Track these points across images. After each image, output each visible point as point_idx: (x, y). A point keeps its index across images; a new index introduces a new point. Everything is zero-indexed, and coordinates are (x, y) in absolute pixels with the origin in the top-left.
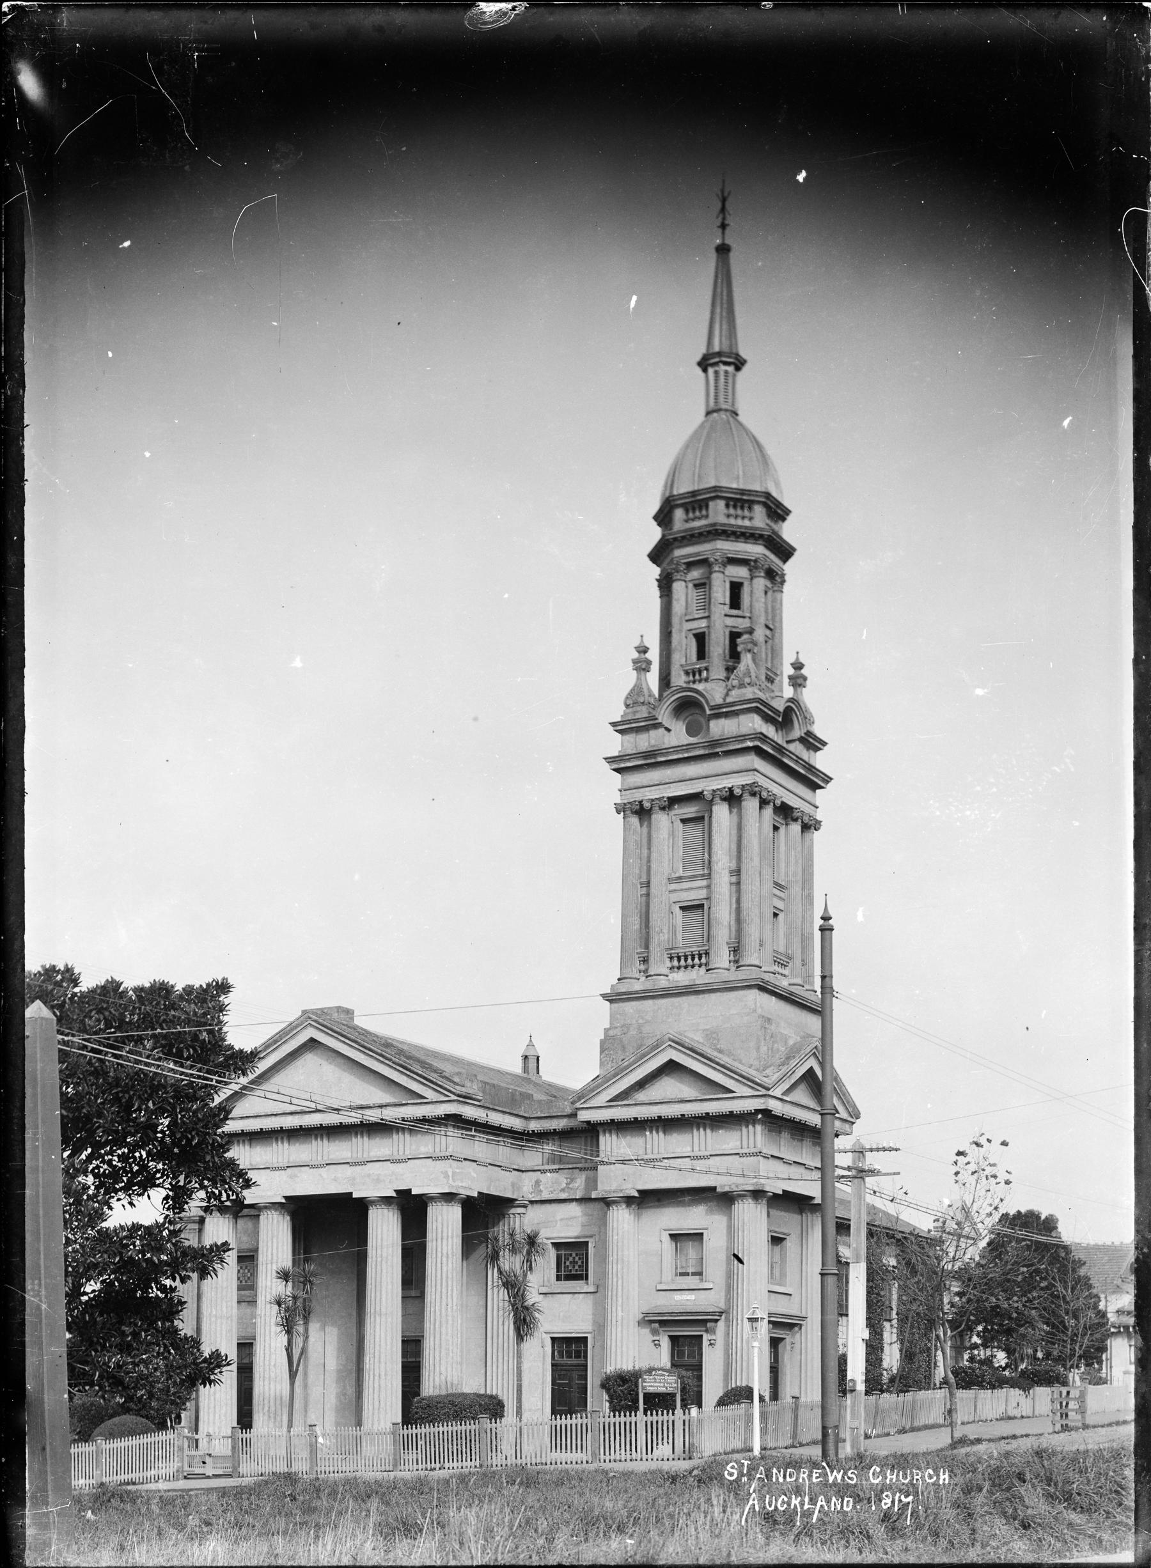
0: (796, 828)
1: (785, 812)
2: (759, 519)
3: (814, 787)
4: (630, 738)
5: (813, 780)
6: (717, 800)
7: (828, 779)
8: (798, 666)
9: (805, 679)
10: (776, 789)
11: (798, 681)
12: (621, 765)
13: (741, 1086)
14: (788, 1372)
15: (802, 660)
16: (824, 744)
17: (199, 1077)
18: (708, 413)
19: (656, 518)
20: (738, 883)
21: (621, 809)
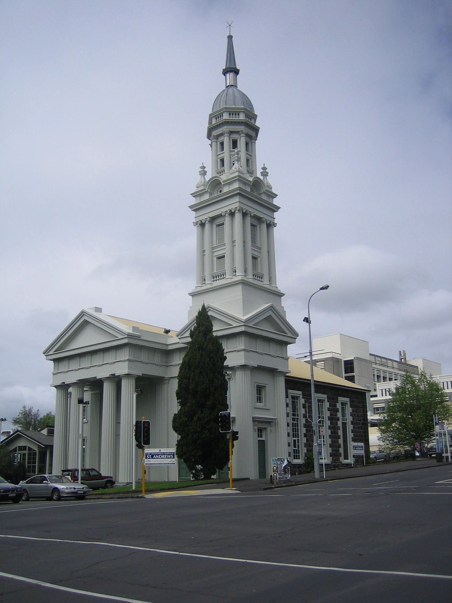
0: (264, 226)
1: (259, 220)
2: (242, 117)
3: (275, 211)
4: (198, 198)
7: (278, 208)
8: (264, 168)
10: (250, 210)
11: (265, 174)
12: (196, 208)
13: (235, 322)
14: (269, 449)
16: (277, 195)
17: (344, 424)
18: (227, 87)
21: (196, 224)
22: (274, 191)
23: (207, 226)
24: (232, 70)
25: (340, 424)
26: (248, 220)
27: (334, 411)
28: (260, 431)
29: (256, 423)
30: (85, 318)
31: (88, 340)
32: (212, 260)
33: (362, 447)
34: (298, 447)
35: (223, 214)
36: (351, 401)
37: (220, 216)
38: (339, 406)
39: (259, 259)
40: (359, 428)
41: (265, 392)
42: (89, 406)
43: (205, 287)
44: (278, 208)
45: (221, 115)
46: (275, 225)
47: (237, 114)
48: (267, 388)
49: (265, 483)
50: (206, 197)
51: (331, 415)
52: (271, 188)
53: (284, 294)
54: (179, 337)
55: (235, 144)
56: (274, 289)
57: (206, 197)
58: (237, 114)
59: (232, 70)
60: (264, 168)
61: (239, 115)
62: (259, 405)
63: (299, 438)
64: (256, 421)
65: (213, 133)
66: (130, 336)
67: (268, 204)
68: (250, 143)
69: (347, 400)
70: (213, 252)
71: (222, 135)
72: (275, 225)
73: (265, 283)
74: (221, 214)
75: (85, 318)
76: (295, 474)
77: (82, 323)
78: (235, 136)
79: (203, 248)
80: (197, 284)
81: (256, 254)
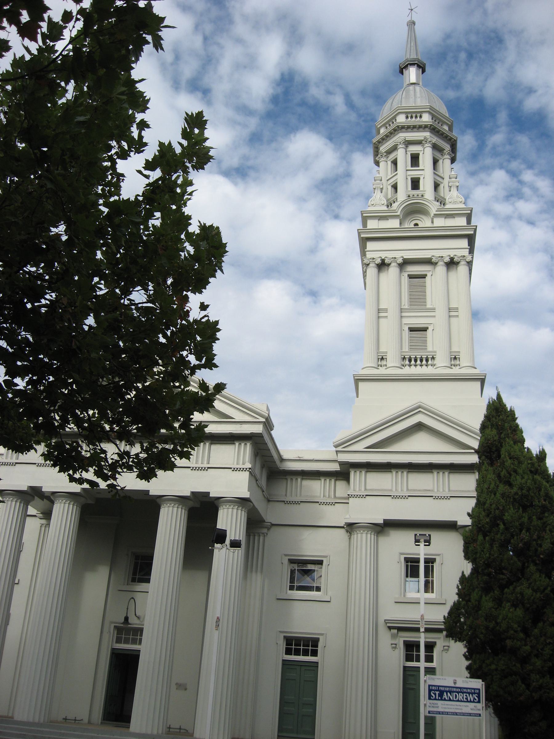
32: (401, 330)
37: (428, 262)
42: (385, 208)
50: (394, 223)
54: (339, 449)
55: (415, 159)
57: (394, 223)
65: (381, 149)
71: (394, 148)
74: (431, 259)
78: (414, 149)
79: (378, 348)
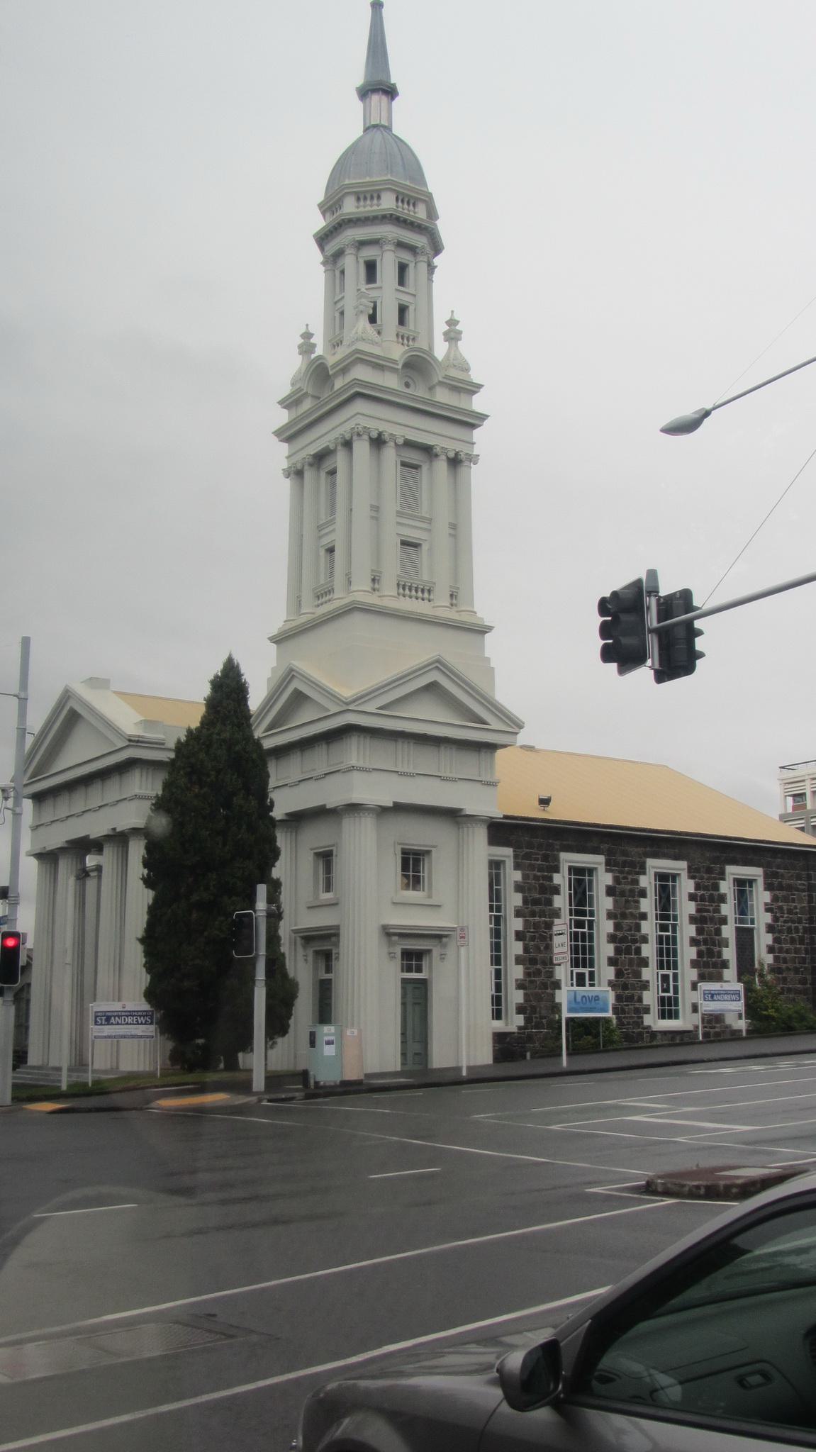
0: (441, 466)
2: (388, 203)
3: (473, 426)
5: (471, 422)
6: (366, 437)
8: (452, 323)
9: (460, 332)
11: (453, 336)
15: (456, 317)
18: (366, 130)
19: (321, 206)
20: (377, 519)
22: (475, 377)
23: (309, 475)
24: (379, 87)
25: (728, 932)
26: (390, 453)
27: (711, 899)
28: (412, 959)
29: (395, 938)
30: (296, 684)
31: (80, 754)
33: (737, 993)
34: (676, 992)
35: (332, 447)
36: (766, 876)
38: (726, 887)
39: (425, 547)
40: (793, 941)
41: (430, 863)
43: (303, 619)
44: (483, 417)
45: (376, 195)
46: (473, 459)
47: (368, 196)
48: (434, 854)
49: (421, 1079)
50: (307, 405)
51: (698, 910)
52: (467, 370)
53: (490, 629)
56: (465, 618)
57: (307, 405)
58: (368, 196)
59: (379, 87)
60: (452, 323)
61: (379, 197)
62: (412, 895)
63: (679, 971)
64: (395, 934)
66: (134, 742)
67: (442, 408)
68: (411, 266)
69: (755, 872)
70: (320, 537)
72: (473, 459)
73: (439, 607)
75: (296, 684)
76: (525, 1057)
77: (69, 718)
78: (369, 253)
80: (288, 613)
81: (412, 534)
